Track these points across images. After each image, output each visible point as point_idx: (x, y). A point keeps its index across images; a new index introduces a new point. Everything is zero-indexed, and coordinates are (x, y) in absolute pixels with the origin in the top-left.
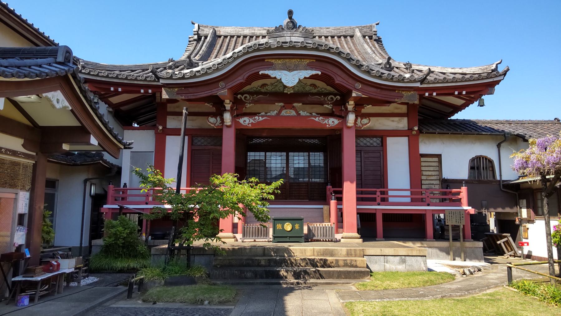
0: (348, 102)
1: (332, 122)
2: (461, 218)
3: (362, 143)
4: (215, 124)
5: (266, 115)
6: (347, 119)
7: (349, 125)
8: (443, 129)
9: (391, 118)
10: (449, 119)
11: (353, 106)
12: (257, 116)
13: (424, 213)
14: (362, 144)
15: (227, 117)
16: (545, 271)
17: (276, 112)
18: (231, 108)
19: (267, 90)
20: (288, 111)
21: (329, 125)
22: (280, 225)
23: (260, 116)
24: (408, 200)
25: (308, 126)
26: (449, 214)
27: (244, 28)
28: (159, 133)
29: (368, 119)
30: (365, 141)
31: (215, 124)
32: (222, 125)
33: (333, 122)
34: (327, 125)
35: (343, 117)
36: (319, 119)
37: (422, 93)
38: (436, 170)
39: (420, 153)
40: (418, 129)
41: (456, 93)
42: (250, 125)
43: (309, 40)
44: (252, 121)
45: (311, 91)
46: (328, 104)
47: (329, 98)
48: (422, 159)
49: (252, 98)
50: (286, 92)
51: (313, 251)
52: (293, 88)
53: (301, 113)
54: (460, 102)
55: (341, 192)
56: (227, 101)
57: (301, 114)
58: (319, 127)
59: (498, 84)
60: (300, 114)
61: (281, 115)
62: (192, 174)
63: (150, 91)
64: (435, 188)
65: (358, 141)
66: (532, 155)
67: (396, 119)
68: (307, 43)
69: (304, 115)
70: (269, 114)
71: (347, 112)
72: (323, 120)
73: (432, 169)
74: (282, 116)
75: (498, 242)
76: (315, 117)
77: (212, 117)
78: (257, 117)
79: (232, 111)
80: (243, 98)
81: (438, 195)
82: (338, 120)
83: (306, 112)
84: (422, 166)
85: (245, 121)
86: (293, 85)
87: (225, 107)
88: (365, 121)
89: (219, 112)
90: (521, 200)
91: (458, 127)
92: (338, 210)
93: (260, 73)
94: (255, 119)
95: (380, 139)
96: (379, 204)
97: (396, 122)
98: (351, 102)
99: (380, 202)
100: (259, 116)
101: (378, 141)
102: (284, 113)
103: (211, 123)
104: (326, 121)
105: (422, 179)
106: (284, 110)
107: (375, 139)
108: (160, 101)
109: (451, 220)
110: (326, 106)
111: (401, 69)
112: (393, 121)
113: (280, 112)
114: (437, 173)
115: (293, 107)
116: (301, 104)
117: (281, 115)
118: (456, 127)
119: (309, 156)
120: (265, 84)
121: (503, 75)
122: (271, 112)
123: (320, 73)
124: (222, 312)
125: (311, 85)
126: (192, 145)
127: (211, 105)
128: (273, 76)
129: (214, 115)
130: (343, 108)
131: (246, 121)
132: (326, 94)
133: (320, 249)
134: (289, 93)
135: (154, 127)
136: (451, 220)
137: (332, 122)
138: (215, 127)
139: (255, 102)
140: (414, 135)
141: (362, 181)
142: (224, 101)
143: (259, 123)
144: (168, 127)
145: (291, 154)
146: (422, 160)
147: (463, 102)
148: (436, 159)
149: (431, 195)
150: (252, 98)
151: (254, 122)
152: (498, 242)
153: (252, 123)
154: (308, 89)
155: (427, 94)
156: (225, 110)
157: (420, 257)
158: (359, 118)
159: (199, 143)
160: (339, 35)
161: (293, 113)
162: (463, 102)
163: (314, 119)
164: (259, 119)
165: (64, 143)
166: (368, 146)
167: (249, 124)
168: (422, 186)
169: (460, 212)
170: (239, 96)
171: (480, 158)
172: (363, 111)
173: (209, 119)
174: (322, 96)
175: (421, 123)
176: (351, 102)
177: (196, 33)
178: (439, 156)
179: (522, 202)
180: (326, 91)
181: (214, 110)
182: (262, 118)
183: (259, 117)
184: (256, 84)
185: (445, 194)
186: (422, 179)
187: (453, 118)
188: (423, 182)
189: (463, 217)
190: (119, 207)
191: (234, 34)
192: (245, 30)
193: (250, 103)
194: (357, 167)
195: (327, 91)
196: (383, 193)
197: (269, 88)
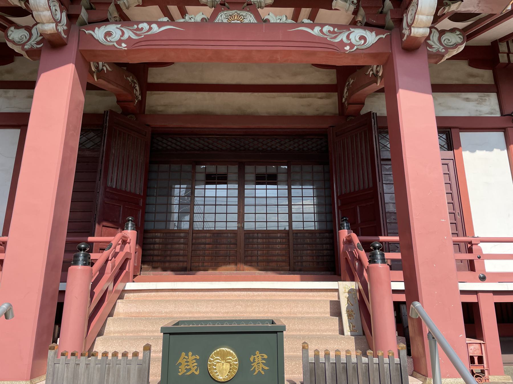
4: (23, 45)
9: (463, 94)
21: (352, 45)
22: (192, 357)
31: (23, 45)
33: (362, 38)
34: (346, 45)
42: (124, 45)
44: (128, 34)
67: (474, 96)
72: (334, 32)
74: (217, 23)
82: (377, 35)
85: (108, 34)
94: (138, 29)
97: (473, 101)
102: (222, 17)
106: (223, 11)
112: (467, 100)
119: (290, 221)
141: (290, 263)
143: (150, 39)
151: (134, 37)
157: (92, 137)
161: (250, 18)
163: (309, 30)
164: (150, 29)
167: (119, 42)
182: (159, 27)
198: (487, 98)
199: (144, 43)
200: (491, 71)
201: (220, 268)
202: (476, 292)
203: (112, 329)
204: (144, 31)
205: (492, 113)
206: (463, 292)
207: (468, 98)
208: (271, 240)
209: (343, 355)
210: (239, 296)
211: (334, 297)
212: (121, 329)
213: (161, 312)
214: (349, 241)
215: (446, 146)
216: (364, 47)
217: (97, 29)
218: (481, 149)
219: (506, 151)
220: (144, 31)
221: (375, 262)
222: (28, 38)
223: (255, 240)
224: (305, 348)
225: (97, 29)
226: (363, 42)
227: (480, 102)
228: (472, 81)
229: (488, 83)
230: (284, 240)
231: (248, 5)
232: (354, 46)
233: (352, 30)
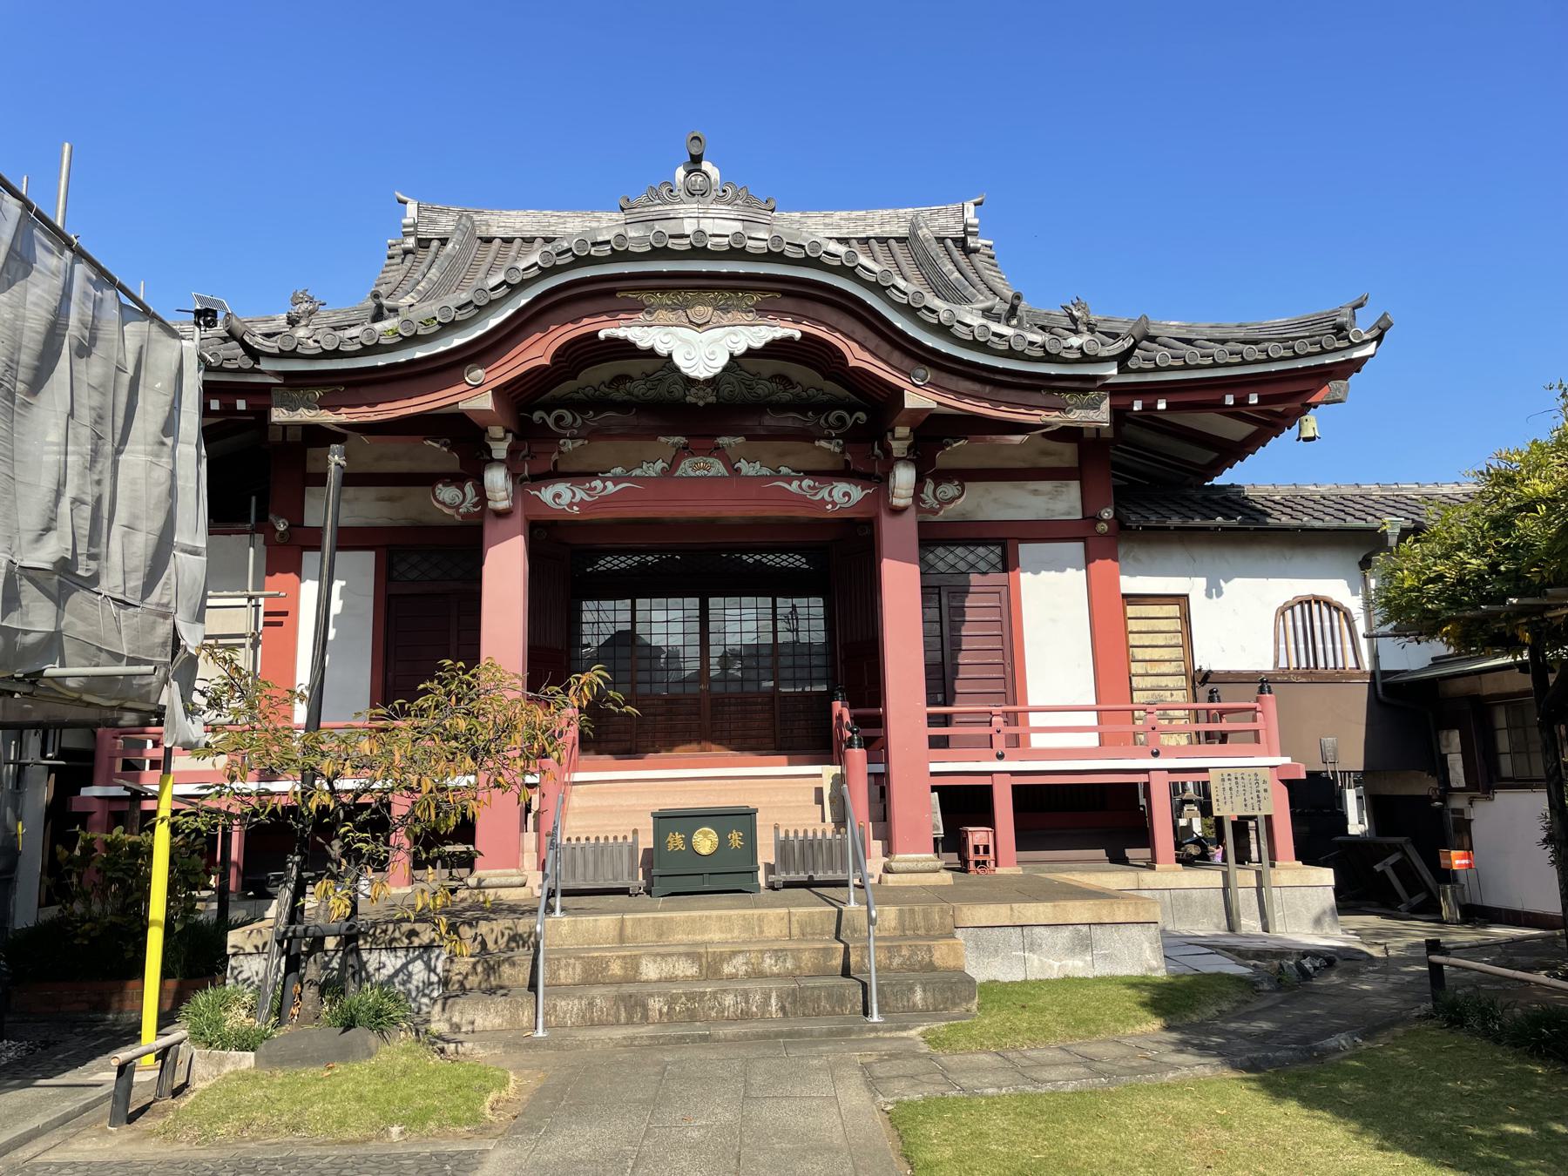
0: (892, 431)
1: (844, 496)
2: (1262, 794)
3: (941, 563)
4: (458, 507)
5: (630, 476)
6: (891, 485)
7: (898, 502)
8: (1190, 514)
10: (1206, 484)
11: (907, 443)
12: (600, 478)
13: (1140, 779)
14: (941, 566)
15: (496, 479)
16: (1537, 958)
17: (660, 465)
18: (512, 451)
19: (629, 393)
20: (700, 460)
21: (834, 504)
23: (608, 479)
24: (1092, 740)
25: (773, 511)
26: (1223, 780)
27: (565, 214)
28: (278, 545)
29: (957, 483)
30: (951, 558)
31: (458, 507)
32: (481, 514)
34: (828, 503)
35: (877, 479)
36: (800, 486)
37: (1122, 401)
38: (1172, 643)
39: (1124, 591)
40: (1115, 517)
41: (1230, 400)
42: (576, 508)
43: (759, 231)
44: (580, 495)
45: (774, 398)
46: (829, 438)
47: (831, 419)
48: (1132, 611)
49: (579, 420)
50: (694, 400)
51: (786, 920)
52: (712, 382)
53: (745, 468)
54: (1239, 430)
55: (879, 722)
56: (496, 431)
57: (744, 472)
58: (801, 513)
59: (1358, 371)
60: (738, 470)
61: (677, 474)
62: (390, 674)
63: (241, 405)
64: (1174, 698)
65: (931, 556)
66: (335, 865)
67: (1046, 486)
68: (750, 238)
69: (752, 473)
70: (637, 472)
71: (890, 463)
73: (1160, 639)
75: (1378, 867)
76: (789, 480)
77: (446, 485)
78: (598, 483)
79: (512, 464)
80: (550, 421)
81: (1183, 722)
83: (758, 465)
84: (1131, 632)
85: (558, 496)
86: (710, 375)
87: (489, 451)
88: (949, 490)
89: (472, 470)
90: (1445, 732)
91: (1237, 507)
92: (872, 779)
93: (602, 335)
95: (998, 550)
96: (1000, 757)
98: (902, 431)
99: (1006, 751)
100: (604, 480)
101: (992, 556)
102: (687, 468)
103: (444, 503)
104: (824, 493)
105: (1133, 672)
106: (688, 457)
107: (981, 550)
108: (280, 438)
109: (1228, 800)
110: (823, 444)
111: (1054, 330)
112: (1035, 492)
113: (674, 464)
114: (1178, 653)
115: (717, 448)
116: (740, 440)
117: (677, 474)
118: (1231, 509)
120: (619, 376)
121: (1373, 340)
122: (645, 466)
123: (798, 335)
124: (448, 1167)
125: (772, 378)
126: (390, 579)
127: (445, 445)
128: (643, 344)
129: (456, 480)
130: (877, 451)
131: (560, 497)
132: (822, 408)
133: (810, 913)
134: (701, 403)
135: (263, 525)
136: (1228, 800)
137: (844, 496)
138: (458, 518)
139: (594, 434)
140: (1102, 535)
142: (487, 431)
143: (605, 500)
144: (306, 524)
145: (714, 602)
146: (1129, 615)
147: (1247, 429)
148: (1174, 610)
149: (1162, 721)
150: (579, 420)
151: (588, 499)
152: (1378, 867)
153: (582, 503)
154: (763, 388)
155: (1138, 406)
156: (492, 460)
158: (928, 480)
159: (413, 575)
160: (864, 235)
161: (718, 468)
162: (1247, 429)
164: (605, 488)
165: (1556, 805)
166: (963, 573)
167: (571, 505)
168: (1135, 693)
169: (1256, 775)
170: (537, 416)
171: (1309, 602)
172: (943, 460)
173: (438, 492)
174: (810, 413)
175: (1122, 498)
176: (902, 431)
177: (412, 229)
178: (1181, 600)
179: (1447, 739)
180: (821, 397)
181: (453, 463)
182: (615, 485)
183: (604, 482)
184: (596, 376)
185: (946, 720)
186: (1133, 672)
187: (1217, 481)
188: (1136, 682)
189: (1266, 790)
190: (128, 794)
191: (535, 234)
192: (568, 219)
193: (572, 438)
194: (927, 639)
195: (825, 398)
196: (1013, 718)
197: (639, 389)
198: (1064, 489)
199: (598, 506)
200: (1076, 445)
201: (677, 749)
202: (990, 773)
203: (573, 824)
204: (598, 490)
205: (1069, 514)
206: (933, 774)
207: (1036, 490)
208: (748, 707)
209: (810, 834)
210: (710, 785)
211: (815, 783)
212: (583, 823)
213: (622, 806)
214: (840, 717)
215: (1000, 566)
216: (847, 505)
217: (543, 489)
218: (1048, 569)
219: (1084, 571)
220: (598, 490)
221: (851, 747)
222: (461, 498)
223: (726, 708)
224: (776, 828)
225: (543, 489)
226: (847, 498)
227: (1054, 496)
228: (1047, 462)
229: (1067, 466)
230: (767, 707)
231: (716, 449)
232: (836, 504)
233: (835, 484)
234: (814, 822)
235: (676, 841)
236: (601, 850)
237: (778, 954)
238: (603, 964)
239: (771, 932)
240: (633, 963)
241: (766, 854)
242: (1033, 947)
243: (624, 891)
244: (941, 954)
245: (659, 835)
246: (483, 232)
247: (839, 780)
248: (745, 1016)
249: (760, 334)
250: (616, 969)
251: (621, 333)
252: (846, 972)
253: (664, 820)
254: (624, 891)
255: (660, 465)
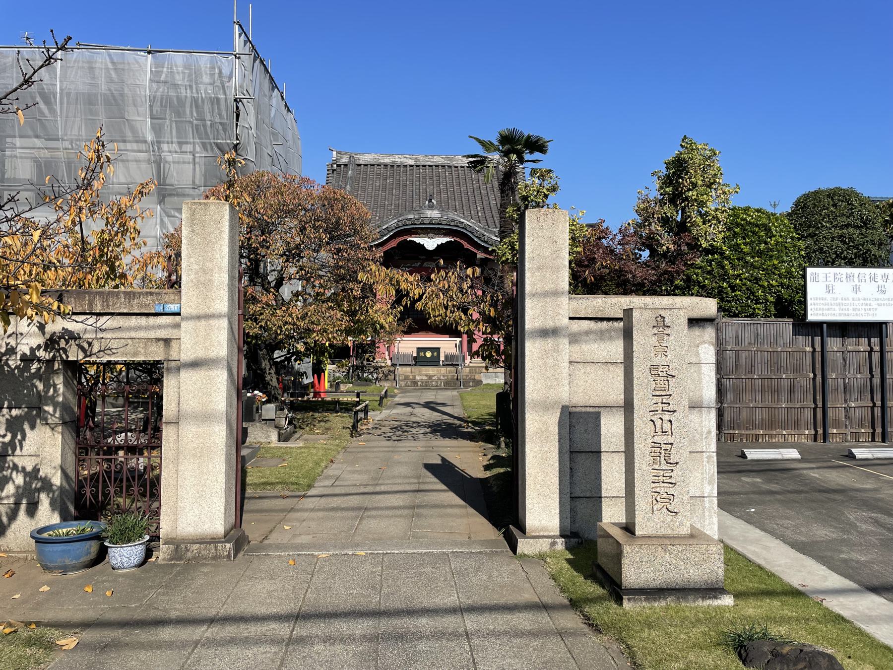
17: (419, 264)
20: (429, 263)
113: (422, 263)
211: (455, 342)
234: (453, 351)
235: (422, 354)
236: (405, 356)
237: (444, 376)
238: (408, 376)
239: (442, 372)
240: (414, 376)
241: (442, 358)
242: (497, 377)
243: (410, 365)
244: (477, 377)
245: (418, 353)
246: (357, 162)
247: (461, 342)
248: (437, 386)
249: (444, 240)
250: (411, 377)
251: (412, 239)
252: (457, 379)
253: (419, 350)
254: (410, 365)
255: (419, 264)
